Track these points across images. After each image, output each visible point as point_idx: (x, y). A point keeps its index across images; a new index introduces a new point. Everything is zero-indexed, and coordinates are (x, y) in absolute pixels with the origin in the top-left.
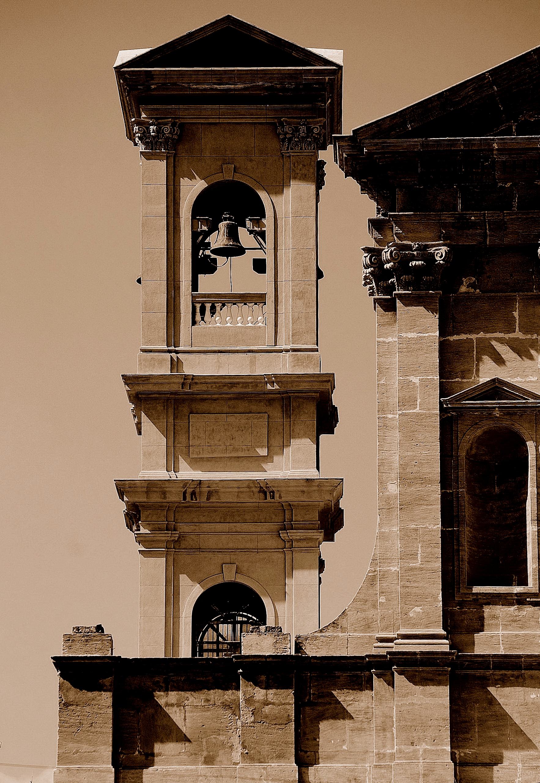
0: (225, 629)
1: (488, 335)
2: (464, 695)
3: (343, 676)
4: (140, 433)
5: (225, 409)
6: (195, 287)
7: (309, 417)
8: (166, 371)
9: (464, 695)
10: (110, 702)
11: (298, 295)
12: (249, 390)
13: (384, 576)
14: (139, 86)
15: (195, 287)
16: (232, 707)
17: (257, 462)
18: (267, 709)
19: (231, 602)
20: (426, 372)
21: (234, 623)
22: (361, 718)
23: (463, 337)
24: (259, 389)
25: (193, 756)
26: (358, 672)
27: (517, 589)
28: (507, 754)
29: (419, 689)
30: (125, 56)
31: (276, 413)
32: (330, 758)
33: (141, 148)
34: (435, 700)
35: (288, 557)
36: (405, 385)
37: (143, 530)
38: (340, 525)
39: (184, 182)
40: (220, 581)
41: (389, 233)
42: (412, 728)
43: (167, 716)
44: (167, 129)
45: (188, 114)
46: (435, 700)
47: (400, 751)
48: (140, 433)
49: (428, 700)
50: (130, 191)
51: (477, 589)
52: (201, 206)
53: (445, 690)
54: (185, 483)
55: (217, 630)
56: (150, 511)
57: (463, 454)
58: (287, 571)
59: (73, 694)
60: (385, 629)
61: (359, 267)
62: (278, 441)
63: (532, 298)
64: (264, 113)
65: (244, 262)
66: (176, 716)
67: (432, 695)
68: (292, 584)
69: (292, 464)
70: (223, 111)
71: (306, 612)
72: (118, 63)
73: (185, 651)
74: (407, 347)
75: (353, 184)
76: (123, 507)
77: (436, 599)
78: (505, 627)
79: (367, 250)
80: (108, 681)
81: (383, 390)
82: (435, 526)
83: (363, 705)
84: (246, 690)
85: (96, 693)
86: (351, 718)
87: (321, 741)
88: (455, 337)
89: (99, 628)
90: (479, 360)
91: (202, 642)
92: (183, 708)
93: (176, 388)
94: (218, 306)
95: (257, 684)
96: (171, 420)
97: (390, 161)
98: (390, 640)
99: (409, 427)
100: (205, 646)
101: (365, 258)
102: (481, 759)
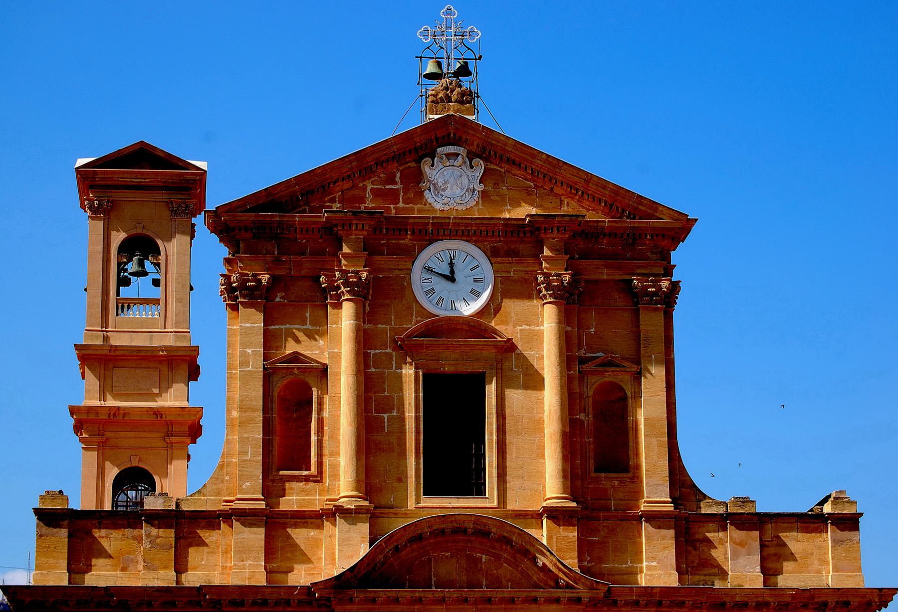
0: (132, 494)
1: (292, 326)
2: (273, 533)
3: (203, 523)
4: (83, 378)
5: (135, 365)
6: (118, 294)
7: (184, 371)
8: (100, 342)
9: (273, 533)
10: (66, 534)
11: (179, 300)
12: (149, 354)
13: (228, 464)
14: (89, 180)
15: (118, 294)
16: (138, 539)
17: (153, 397)
18: (158, 540)
19: (135, 478)
20: (255, 347)
21: (137, 490)
22: (213, 546)
23: (277, 327)
24: (155, 353)
25: (115, 567)
26: (212, 520)
27: (305, 473)
28: (296, 566)
29: (247, 529)
30: (81, 162)
31: (165, 369)
32: (194, 569)
33: (89, 213)
34: (256, 536)
35: (170, 453)
36: (243, 354)
37: (84, 435)
38: (200, 434)
39: (114, 234)
40: (129, 466)
41: (235, 266)
42: (243, 552)
43: (99, 543)
44: (105, 204)
45: (117, 195)
46: (256, 536)
47: (235, 565)
48: (83, 378)
49: (253, 536)
50: (79, 239)
51: (281, 473)
52: (122, 248)
53: (262, 530)
54: (110, 408)
55: (127, 495)
56: (86, 422)
57: (276, 394)
58: (168, 461)
59: (45, 530)
60: (229, 495)
61: (218, 284)
62: (164, 386)
63: (317, 306)
64: (163, 196)
65: (147, 280)
66: (105, 544)
67: (255, 533)
68: (171, 468)
69: (173, 399)
70: (137, 192)
71: (183, 482)
72: (77, 165)
73: (108, 506)
74: (245, 332)
75: (215, 238)
76: (72, 421)
77: (258, 479)
78: (298, 494)
79: (222, 275)
80: (65, 523)
81: (230, 356)
82: (260, 436)
83: (214, 538)
84: (146, 530)
85: (58, 529)
86: (207, 546)
87: (189, 559)
88: (273, 327)
89: (61, 492)
90: (286, 340)
91: (117, 501)
92: (109, 539)
93: (105, 352)
94: (132, 305)
95: (152, 526)
96: (102, 371)
97: (232, 225)
98: (232, 501)
99: (246, 378)
100: (119, 504)
101: (221, 280)
102: (281, 570)
